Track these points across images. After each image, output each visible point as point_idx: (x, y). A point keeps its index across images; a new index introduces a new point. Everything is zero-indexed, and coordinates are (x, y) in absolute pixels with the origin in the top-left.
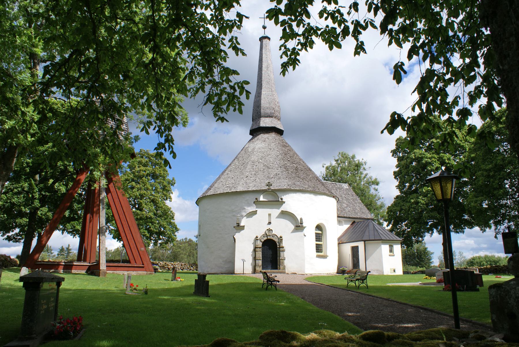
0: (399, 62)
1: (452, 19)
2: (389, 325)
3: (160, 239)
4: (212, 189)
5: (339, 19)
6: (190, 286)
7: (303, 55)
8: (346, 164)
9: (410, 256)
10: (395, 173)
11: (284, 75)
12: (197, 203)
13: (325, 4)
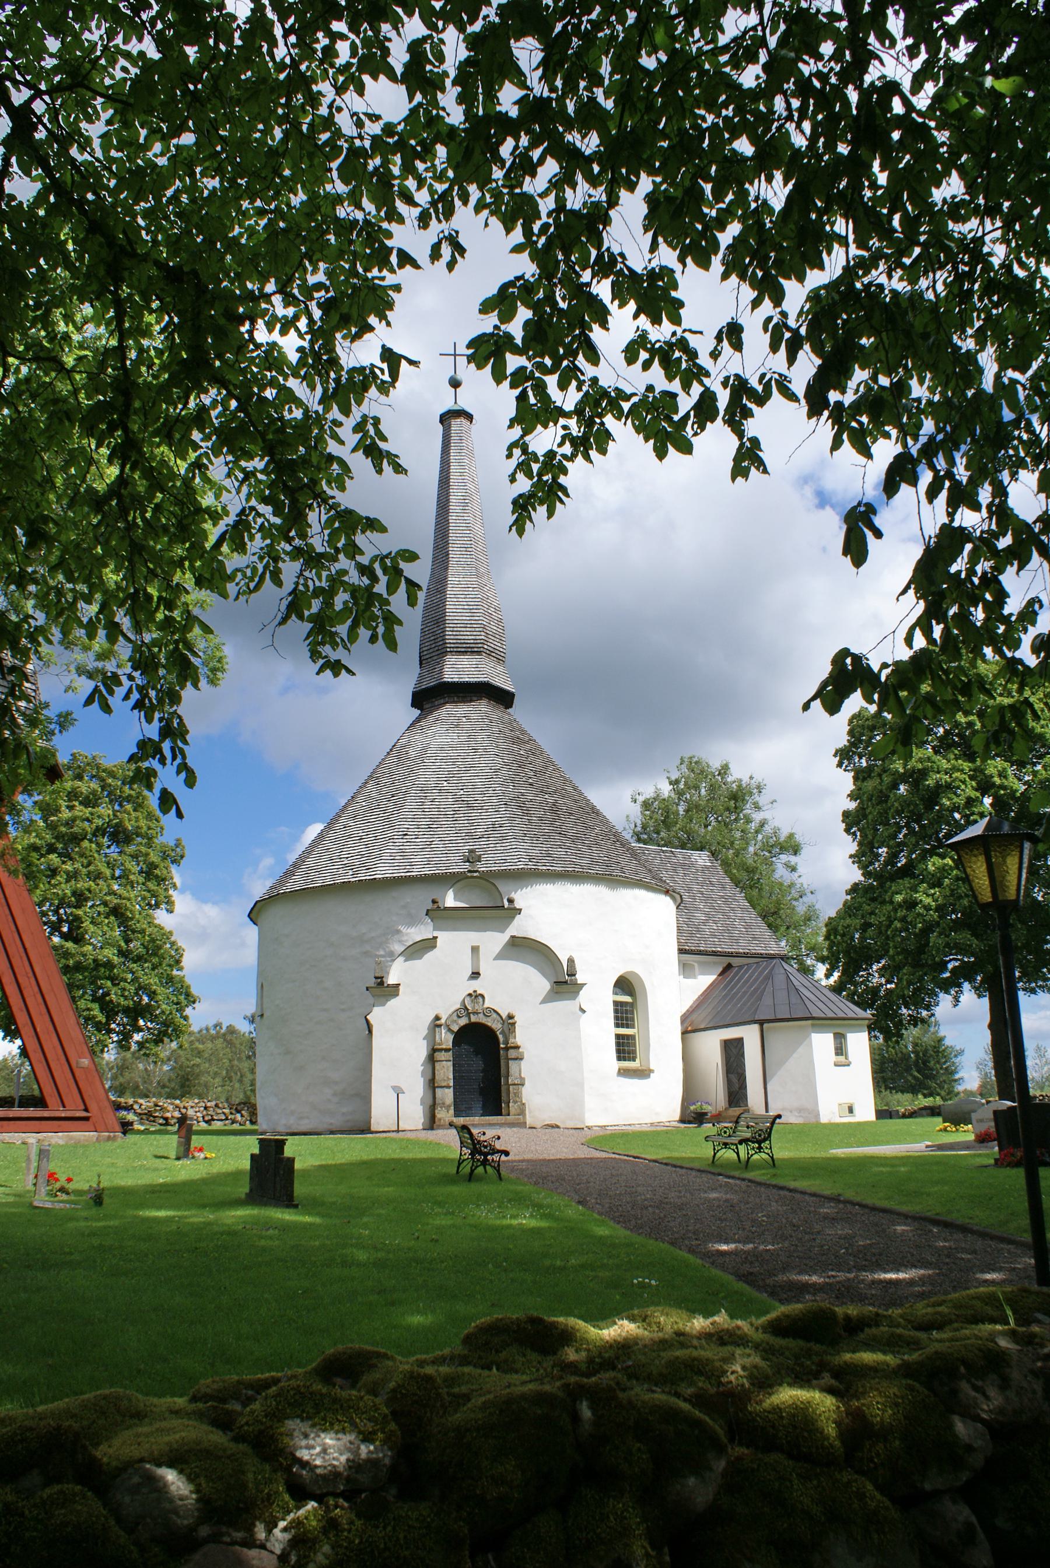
0: (859, 504)
1: (1011, 373)
2: (842, 1276)
3: (139, 1030)
4: (299, 872)
5: (684, 365)
6: (236, 1174)
7: (577, 474)
8: (703, 792)
9: (896, 1064)
10: (846, 815)
11: (521, 532)
12: (254, 915)
13: (643, 321)
